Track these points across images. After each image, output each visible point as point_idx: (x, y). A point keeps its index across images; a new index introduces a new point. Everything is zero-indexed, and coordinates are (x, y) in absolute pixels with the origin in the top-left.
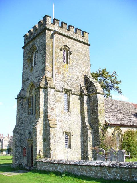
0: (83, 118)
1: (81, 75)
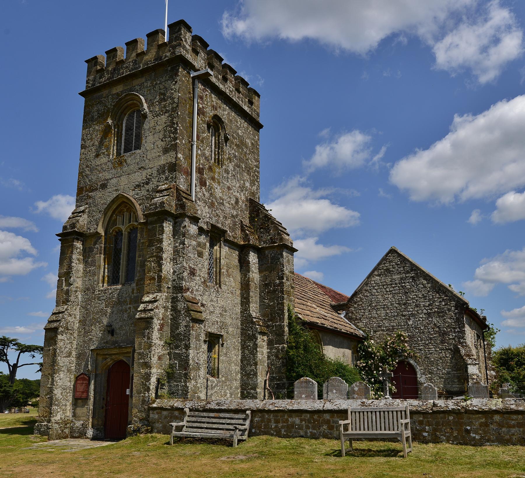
0: (245, 301)
1: (243, 198)
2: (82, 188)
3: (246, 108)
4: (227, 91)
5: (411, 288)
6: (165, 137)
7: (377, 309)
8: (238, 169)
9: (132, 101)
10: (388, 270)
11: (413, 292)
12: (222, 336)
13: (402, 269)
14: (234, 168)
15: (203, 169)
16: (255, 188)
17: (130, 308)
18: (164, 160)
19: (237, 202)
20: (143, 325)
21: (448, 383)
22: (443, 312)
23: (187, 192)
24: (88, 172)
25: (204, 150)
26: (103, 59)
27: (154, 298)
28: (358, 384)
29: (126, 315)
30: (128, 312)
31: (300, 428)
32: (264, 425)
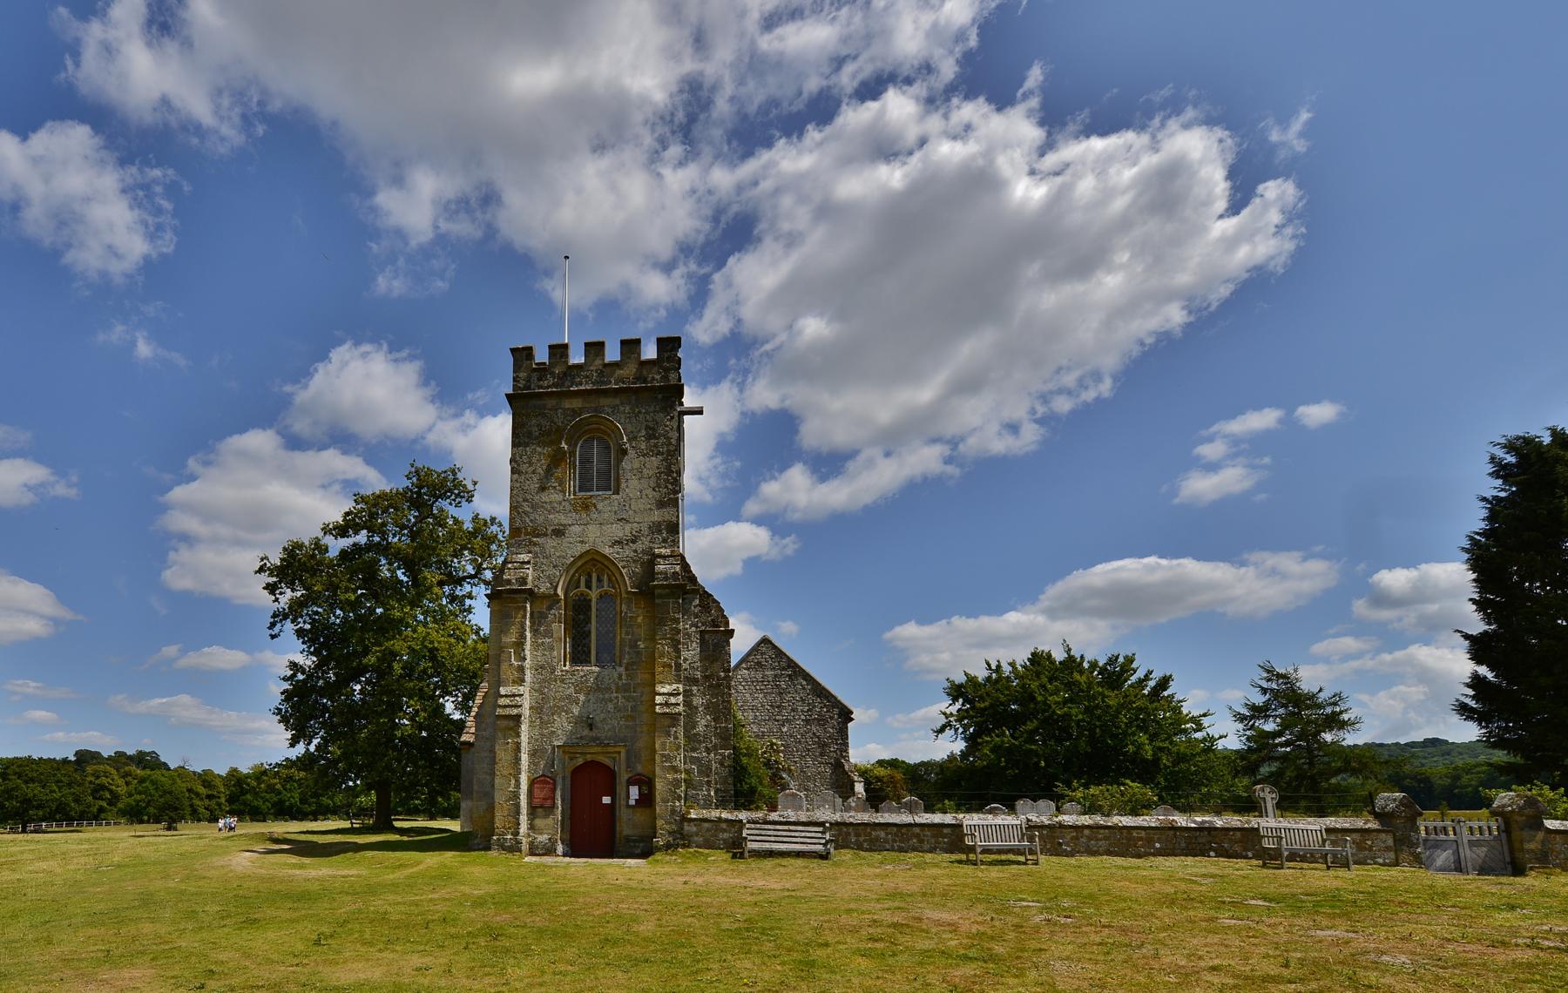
10: (759, 664)
18: (657, 516)
20: (667, 722)
26: (541, 356)
29: (610, 706)
31: (886, 841)
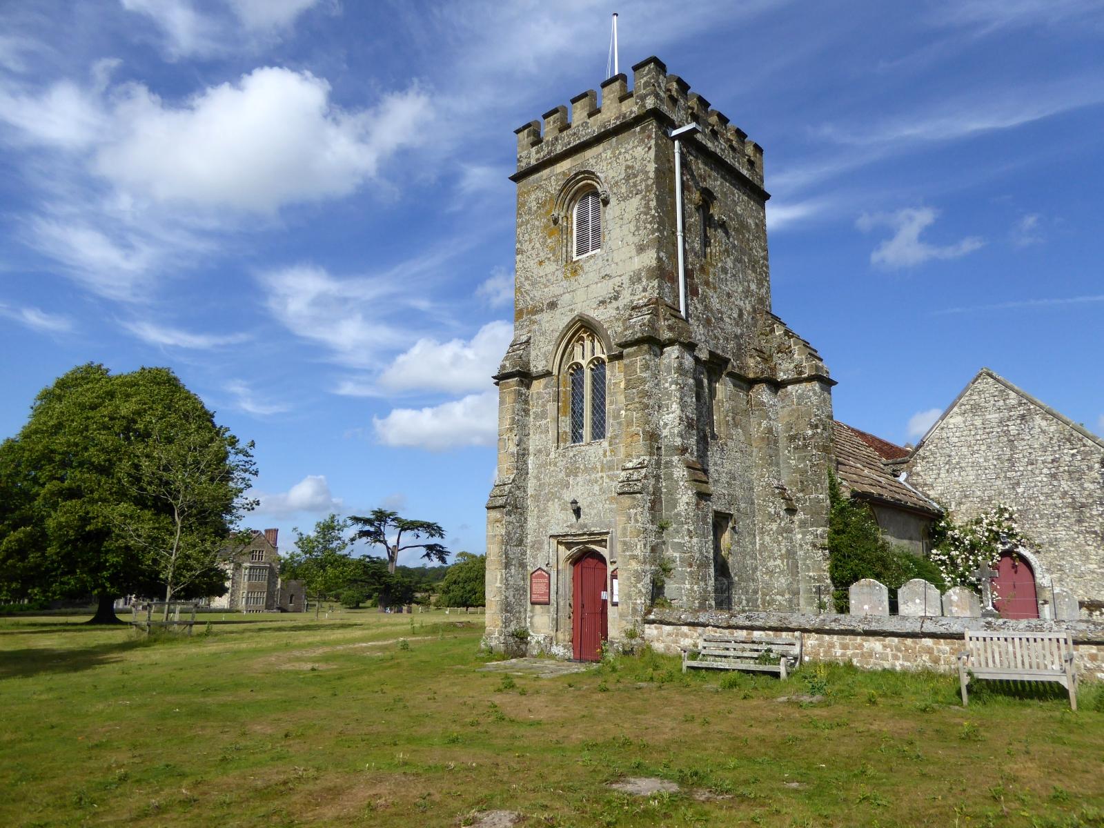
1: (749, 308)
2: (521, 310)
3: (745, 172)
4: (718, 151)
5: (1019, 434)
6: (638, 229)
7: (961, 467)
8: (739, 265)
9: (589, 182)
11: (1023, 439)
12: (732, 515)
13: (1001, 403)
14: (734, 264)
15: (692, 270)
16: (763, 291)
17: (602, 477)
19: (741, 315)
21: (1093, 587)
22: (1079, 471)
23: (673, 306)
24: (528, 287)
25: (693, 242)
27: (640, 463)
28: (958, 591)
29: (596, 488)
30: (599, 483)
32: (824, 652)
